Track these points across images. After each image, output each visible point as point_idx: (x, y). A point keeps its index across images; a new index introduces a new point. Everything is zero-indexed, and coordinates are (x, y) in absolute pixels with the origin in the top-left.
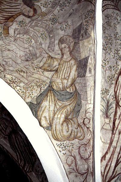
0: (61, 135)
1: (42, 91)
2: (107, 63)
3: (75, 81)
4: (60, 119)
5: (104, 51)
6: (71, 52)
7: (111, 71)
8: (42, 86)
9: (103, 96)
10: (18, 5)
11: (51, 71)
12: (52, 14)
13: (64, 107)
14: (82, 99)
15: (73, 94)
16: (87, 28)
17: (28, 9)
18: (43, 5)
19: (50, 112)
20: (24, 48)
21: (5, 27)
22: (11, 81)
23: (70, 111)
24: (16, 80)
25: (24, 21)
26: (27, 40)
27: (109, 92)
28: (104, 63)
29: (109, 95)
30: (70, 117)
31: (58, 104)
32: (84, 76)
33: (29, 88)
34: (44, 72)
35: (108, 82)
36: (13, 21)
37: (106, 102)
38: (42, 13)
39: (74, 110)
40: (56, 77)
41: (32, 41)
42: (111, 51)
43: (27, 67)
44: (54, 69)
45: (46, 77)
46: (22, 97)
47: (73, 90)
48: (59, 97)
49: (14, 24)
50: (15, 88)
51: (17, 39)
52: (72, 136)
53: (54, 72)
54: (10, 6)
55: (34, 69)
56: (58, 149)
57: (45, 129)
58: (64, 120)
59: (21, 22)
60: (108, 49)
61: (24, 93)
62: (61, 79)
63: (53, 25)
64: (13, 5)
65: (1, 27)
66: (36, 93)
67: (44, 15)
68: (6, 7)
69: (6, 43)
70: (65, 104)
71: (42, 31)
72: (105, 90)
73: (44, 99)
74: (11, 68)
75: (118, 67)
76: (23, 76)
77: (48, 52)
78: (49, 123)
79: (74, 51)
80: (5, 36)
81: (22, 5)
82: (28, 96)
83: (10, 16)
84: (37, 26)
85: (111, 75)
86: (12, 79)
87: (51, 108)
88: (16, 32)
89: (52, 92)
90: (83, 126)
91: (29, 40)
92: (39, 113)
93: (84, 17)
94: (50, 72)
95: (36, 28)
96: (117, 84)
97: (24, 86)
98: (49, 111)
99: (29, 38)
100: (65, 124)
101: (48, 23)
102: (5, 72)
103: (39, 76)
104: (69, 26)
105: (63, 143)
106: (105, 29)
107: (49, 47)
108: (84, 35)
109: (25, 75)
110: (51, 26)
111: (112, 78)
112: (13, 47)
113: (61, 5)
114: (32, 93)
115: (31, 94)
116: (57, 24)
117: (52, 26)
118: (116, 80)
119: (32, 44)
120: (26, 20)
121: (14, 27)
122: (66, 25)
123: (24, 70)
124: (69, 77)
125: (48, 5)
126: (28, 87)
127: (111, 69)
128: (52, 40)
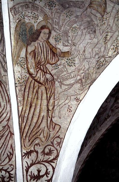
12: (45, 9)
17: (42, 35)
18: (36, 21)
21: (62, 56)
22: (116, 50)
24: (115, 45)
34: (107, 12)
36: (56, 49)
41: (74, 27)
43: (101, 32)
51: (73, 43)
55: (104, 24)
65: (62, 60)
67: (46, 17)
68: (42, 56)
69: (77, 54)
71: (63, 17)
74: (103, 49)
77: (85, 8)
80: (71, 56)
81: (39, 42)
83: (51, 52)
84: (58, 23)
86: (114, 49)
88: (66, 44)
91: (74, 30)
95: (61, 23)
99: (72, 30)
102: (106, 56)
103: (111, 18)
109: (109, 34)
110: (57, 7)
112: (81, 47)
117: (57, 5)
119: (78, 27)
121: (61, 47)
123: (104, 36)
125: (36, 15)
128: (72, 4)
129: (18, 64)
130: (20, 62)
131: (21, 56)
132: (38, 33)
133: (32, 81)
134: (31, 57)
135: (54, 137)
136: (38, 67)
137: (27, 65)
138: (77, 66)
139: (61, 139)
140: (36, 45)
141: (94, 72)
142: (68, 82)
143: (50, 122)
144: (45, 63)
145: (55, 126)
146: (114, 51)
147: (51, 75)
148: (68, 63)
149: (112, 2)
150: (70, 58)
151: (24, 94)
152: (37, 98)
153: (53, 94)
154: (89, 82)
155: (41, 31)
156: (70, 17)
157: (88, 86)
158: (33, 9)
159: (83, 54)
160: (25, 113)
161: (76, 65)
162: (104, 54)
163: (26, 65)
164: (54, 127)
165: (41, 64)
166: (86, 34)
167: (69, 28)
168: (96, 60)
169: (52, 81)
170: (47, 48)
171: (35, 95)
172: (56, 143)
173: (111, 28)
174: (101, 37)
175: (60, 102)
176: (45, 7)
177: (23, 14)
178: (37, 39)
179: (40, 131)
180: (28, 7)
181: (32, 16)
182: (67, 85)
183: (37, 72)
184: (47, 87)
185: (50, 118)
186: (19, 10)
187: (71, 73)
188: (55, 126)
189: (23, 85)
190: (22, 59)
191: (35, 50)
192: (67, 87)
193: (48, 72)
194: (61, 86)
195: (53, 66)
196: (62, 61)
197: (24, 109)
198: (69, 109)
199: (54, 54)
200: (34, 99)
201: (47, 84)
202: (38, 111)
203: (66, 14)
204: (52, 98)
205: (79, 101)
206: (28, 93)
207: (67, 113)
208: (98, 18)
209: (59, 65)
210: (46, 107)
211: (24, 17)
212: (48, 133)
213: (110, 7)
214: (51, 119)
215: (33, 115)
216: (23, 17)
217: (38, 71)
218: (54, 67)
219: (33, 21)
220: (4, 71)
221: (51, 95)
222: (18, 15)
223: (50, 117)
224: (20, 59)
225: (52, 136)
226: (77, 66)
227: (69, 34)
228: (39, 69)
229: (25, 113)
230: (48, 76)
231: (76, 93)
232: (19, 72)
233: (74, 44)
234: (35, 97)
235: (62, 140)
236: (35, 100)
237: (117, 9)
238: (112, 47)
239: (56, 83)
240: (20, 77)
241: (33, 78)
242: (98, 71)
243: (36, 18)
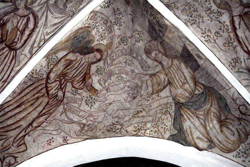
0: (229, 144)
1: (173, 114)
2: (209, 34)
3: (195, 78)
4: (215, 128)
5: (194, 25)
6: (166, 54)
7: (221, 36)
8: (169, 109)
9: (237, 69)
10: (81, 61)
11: (164, 88)
12: (116, 38)
13: (208, 112)
14: (218, 91)
15: (205, 92)
16: (158, 21)
18: (100, 40)
19: (199, 128)
20: (122, 89)
21: (88, 88)
23: (218, 112)
24: (140, 126)
25: (99, 67)
26: (117, 79)
27: (240, 59)
28: (206, 36)
29: (243, 62)
30: (223, 118)
31: (199, 114)
32: (199, 66)
33: (158, 122)
35: (229, 49)
36: (90, 77)
37: (246, 72)
38: (106, 46)
39: (220, 107)
40: (174, 89)
42: (203, 17)
43: (139, 104)
44: (166, 85)
45: (165, 97)
46: (159, 137)
47: (201, 88)
48: (195, 107)
50: (146, 134)
52: (243, 135)
53: (169, 86)
54: (75, 69)
55: (148, 100)
56: (240, 160)
57: (208, 150)
58: (220, 125)
59: (98, 71)
60: (197, 19)
61: (157, 132)
62: (181, 87)
63: (127, 44)
65: (85, 91)
66: (169, 122)
67: (109, 45)
68: (73, 72)
69: (102, 100)
70: (207, 109)
72: (232, 61)
73: (182, 121)
74: (127, 118)
75: (225, 24)
76: (144, 116)
77: (145, 73)
78: (207, 140)
79: (167, 50)
81: (84, 58)
82: (164, 131)
84: (114, 60)
85: (225, 40)
86: (136, 128)
87: (195, 124)
88: (102, 83)
89: (183, 107)
90: (244, 117)
91: (119, 78)
92: (188, 140)
93: (145, 12)
94: (164, 90)
95: (115, 62)
96: (242, 43)
97: (152, 125)
98: (197, 128)
100: (225, 129)
101: (121, 48)
102: (124, 127)
103: (158, 102)
104: (141, 32)
105: (240, 150)
106: (175, 5)
107: (142, 68)
108: (161, 29)
109: (144, 113)
110: (126, 47)
111: (230, 41)
113: (116, 22)
114: (165, 125)
115: (165, 126)
116: (129, 40)
117: (127, 46)
118: (236, 40)
119: (125, 79)
120: (100, 65)
121: (95, 81)
122: (138, 34)
123: (139, 110)
124: (186, 79)
126: (156, 122)
127: (220, 34)
129: (48, 59)
130: (51, 58)
131: (57, 55)
132: (91, 51)
133: (43, 84)
134: (64, 63)
135: (11, 154)
136: (60, 77)
137: (53, 67)
138: (93, 110)
139: (16, 162)
140: (79, 58)
141: (102, 131)
142: (71, 116)
143: (22, 137)
144: (70, 80)
145: (23, 144)
146: (135, 130)
147: (64, 95)
148: (88, 99)
149: (171, 92)
150: (93, 97)
151: (25, 89)
152: (32, 104)
153: (49, 113)
155: (94, 52)
156: (127, 66)
157: (85, 137)
158: (108, 28)
159: (107, 105)
160: (8, 106)
161: (92, 108)
162: (124, 124)
163: (52, 66)
164: (21, 145)
165: (65, 77)
166: (125, 92)
167: (117, 72)
168: (113, 122)
169: (59, 101)
170: (84, 69)
172: (8, 161)
173: (151, 110)
174: (135, 107)
175: (48, 127)
176: (118, 37)
177: (97, 25)
178: (85, 54)
179: (4, 137)
180: (106, 24)
181: (101, 34)
182: (69, 118)
183: (55, 81)
184: (50, 102)
185: (26, 133)
186: (97, 18)
187: (81, 110)
188: (23, 144)
189: (32, 80)
190: (55, 58)
191: (73, 61)
192: (66, 119)
193: (63, 90)
194: (62, 114)
195: (73, 89)
197: (11, 103)
198: (49, 141)
199: (84, 80)
200: (29, 102)
201: (52, 100)
202: (21, 117)
203: (127, 60)
205: (65, 142)
206: (29, 91)
208: (147, 91)
209: (78, 93)
210: (31, 120)
211: (95, 27)
212: (9, 145)
213: (165, 93)
214: (25, 136)
215: (14, 115)
216: (94, 26)
217: (57, 81)
218: (73, 91)
219: (97, 38)
220: (29, 51)
221: (47, 113)
222: (93, 21)
223: (25, 132)
224: (54, 56)
225: (10, 151)
227: (112, 77)
228: (59, 80)
229: (8, 106)
230: (60, 94)
231: (69, 133)
232: (42, 66)
233: (107, 89)
234: (32, 100)
235: (16, 164)
236: (29, 104)
237: (169, 101)
238: (136, 125)
239: (62, 107)
240: (37, 71)
241: (47, 82)
242: (107, 133)
243: (102, 37)
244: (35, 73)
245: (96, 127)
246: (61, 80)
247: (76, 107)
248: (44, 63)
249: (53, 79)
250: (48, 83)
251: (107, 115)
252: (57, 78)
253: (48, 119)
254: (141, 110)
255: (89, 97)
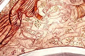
21: (36, 16)
24: (70, 39)
26: (55, 9)
36: (37, 9)
43: (69, 25)
46: (82, 47)
49: (39, 9)
61: (81, 43)
64: (28, 3)
65: (34, 18)
68: (26, 7)
74: (61, 34)
76: (72, 33)
77: (73, 4)
88: (45, 11)
91: (56, 8)
102: (60, 40)
119: (60, 9)
123: (69, 28)
136: (18, 11)
137: (13, 7)
138: (39, 29)
142: (26, 35)
150: (40, 21)
153: (12, 35)
154: (39, 45)
163: (13, 6)
171: (2, 28)
182: (24, 36)
183: (15, 14)
193: (20, 19)
194: (20, 34)
195: (27, 17)
196: (34, 19)
198: (13, 52)
201: (13, 26)
204: (9, 38)
207: (10, 54)
226: (39, 29)
228: (17, 13)
230: (19, 21)
238: (68, 39)
239: (20, 29)
240: (4, 11)
241: (10, 16)
244: (2, 13)
245: (42, 41)
246: (19, 13)
247: (29, 29)
248: (8, 6)
249: (14, 13)
250: (11, 16)
251: (49, 32)
252: (16, 12)
253: (11, 39)
254: (71, 28)
255: (37, 21)
